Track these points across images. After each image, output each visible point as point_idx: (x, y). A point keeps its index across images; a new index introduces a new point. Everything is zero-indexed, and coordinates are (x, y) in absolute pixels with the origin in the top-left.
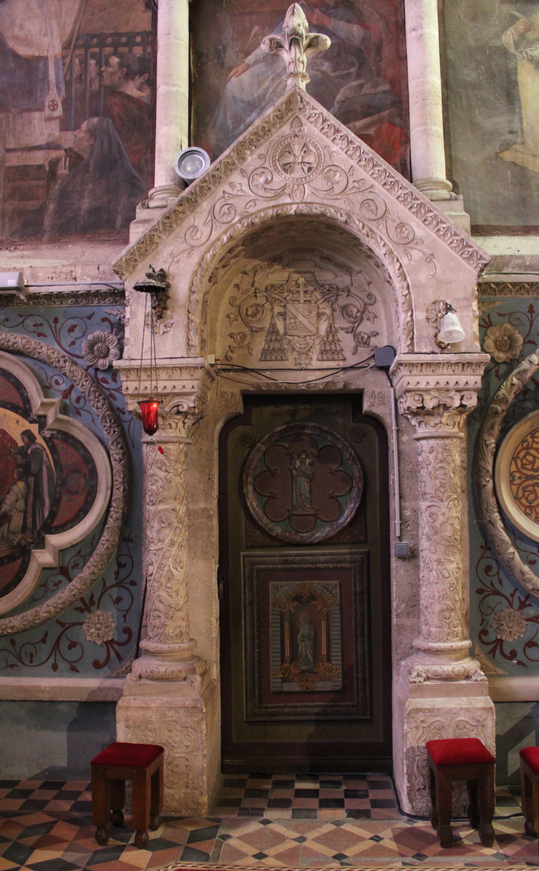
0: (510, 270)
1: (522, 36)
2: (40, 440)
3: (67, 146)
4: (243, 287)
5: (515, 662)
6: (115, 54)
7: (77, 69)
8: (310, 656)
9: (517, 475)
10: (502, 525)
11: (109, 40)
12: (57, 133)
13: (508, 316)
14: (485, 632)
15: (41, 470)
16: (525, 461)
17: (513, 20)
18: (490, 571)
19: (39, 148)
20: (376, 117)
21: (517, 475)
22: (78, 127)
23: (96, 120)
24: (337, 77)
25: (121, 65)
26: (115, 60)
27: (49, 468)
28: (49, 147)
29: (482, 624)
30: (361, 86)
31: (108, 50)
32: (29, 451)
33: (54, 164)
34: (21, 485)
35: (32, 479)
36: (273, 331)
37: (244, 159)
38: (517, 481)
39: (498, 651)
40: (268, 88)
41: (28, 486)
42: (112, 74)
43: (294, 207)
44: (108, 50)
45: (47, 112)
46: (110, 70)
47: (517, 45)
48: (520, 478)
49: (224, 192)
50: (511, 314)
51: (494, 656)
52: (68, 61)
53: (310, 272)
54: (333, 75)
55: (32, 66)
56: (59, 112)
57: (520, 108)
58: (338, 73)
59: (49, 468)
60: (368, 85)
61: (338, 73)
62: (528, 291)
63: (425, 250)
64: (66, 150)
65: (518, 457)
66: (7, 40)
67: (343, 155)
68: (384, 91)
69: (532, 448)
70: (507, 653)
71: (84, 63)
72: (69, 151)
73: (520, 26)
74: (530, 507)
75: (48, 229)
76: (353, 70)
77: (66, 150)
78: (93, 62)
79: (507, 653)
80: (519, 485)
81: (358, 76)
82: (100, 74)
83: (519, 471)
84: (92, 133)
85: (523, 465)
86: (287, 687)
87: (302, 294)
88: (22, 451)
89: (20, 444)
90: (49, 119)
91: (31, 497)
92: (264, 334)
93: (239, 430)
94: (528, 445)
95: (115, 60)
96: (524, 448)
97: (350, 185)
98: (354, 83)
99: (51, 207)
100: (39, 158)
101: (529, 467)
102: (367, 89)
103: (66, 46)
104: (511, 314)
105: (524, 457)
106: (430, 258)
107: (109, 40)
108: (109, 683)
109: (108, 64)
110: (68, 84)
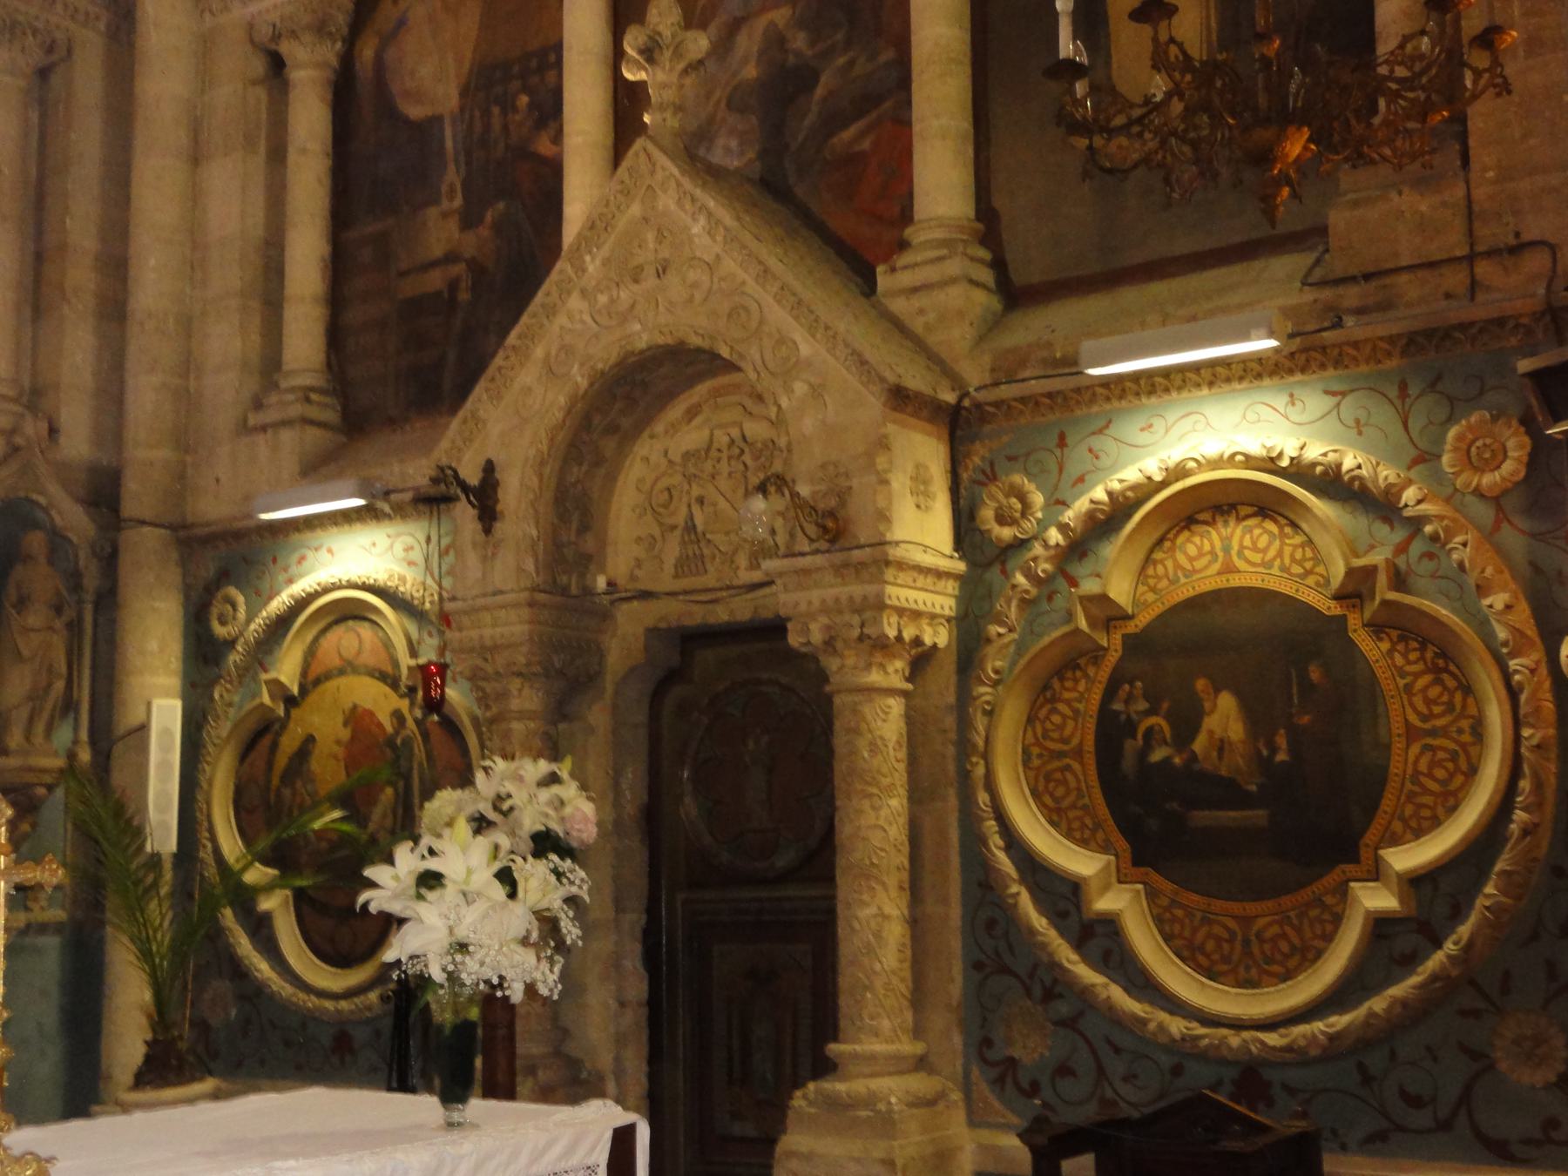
2: (410, 723)
4: (653, 458)
5: (1037, 1102)
7: (478, 126)
8: (769, 1076)
9: (1035, 751)
10: (1001, 843)
11: (516, 69)
14: (987, 1042)
15: (411, 769)
16: (1450, 765)
18: (431, 888)
19: (434, 264)
20: (874, 115)
21: (1035, 751)
22: (481, 221)
23: (501, 205)
27: (421, 764)
28: (450, 258)
29: (982, 1027)
30: (851, 63)
31: (516, 84)
32: (399, 741)
33: (453, 285)
34: (389, 791)
35: (401, 784)
36: (690, 527)
37: (584, 270)
38: (1036, 762)
39: (1009, 1080)
41: (396, 790)
43: (645, 337)
44: (516, 84)
45: (445, 204)
46: (518, 118)
48: (1040, 756)
49: (562, 328)
51: (1002, 1089)
53: (734, 424)
55: (426, 130)
56: (458, 202)
59: (421, 764)
63: (812, 380)
65: (1075, 720)
66: (398, 101)
67: (706, 240)
69: (1060, 700)
70: (1025, 1085)
71: (486, 113)
74: (1059, 811)
78: (496, 110)
79: (1025, 1085)
80: (1038, 769)
82: (505, 128)
83: (1038, 743)
85: (1045, 731)
86: (738, 1129)
87: (724, 462)
88: (390, 742)
89: (389, 729)
90: (445, 215)
91: (400, 811)
92: (678, 533)
93: (677, 692)
94: (1053, 695)
95: (524, 100)
96: (1047, 701)
97: (715, 287)
98: (841, 61)
100: (435, 281)
101: (1441, 755)
103: (464, 92)
105: (1452, 776)
106: (817, 392)
107: (516, 69)
109: (515, 109)
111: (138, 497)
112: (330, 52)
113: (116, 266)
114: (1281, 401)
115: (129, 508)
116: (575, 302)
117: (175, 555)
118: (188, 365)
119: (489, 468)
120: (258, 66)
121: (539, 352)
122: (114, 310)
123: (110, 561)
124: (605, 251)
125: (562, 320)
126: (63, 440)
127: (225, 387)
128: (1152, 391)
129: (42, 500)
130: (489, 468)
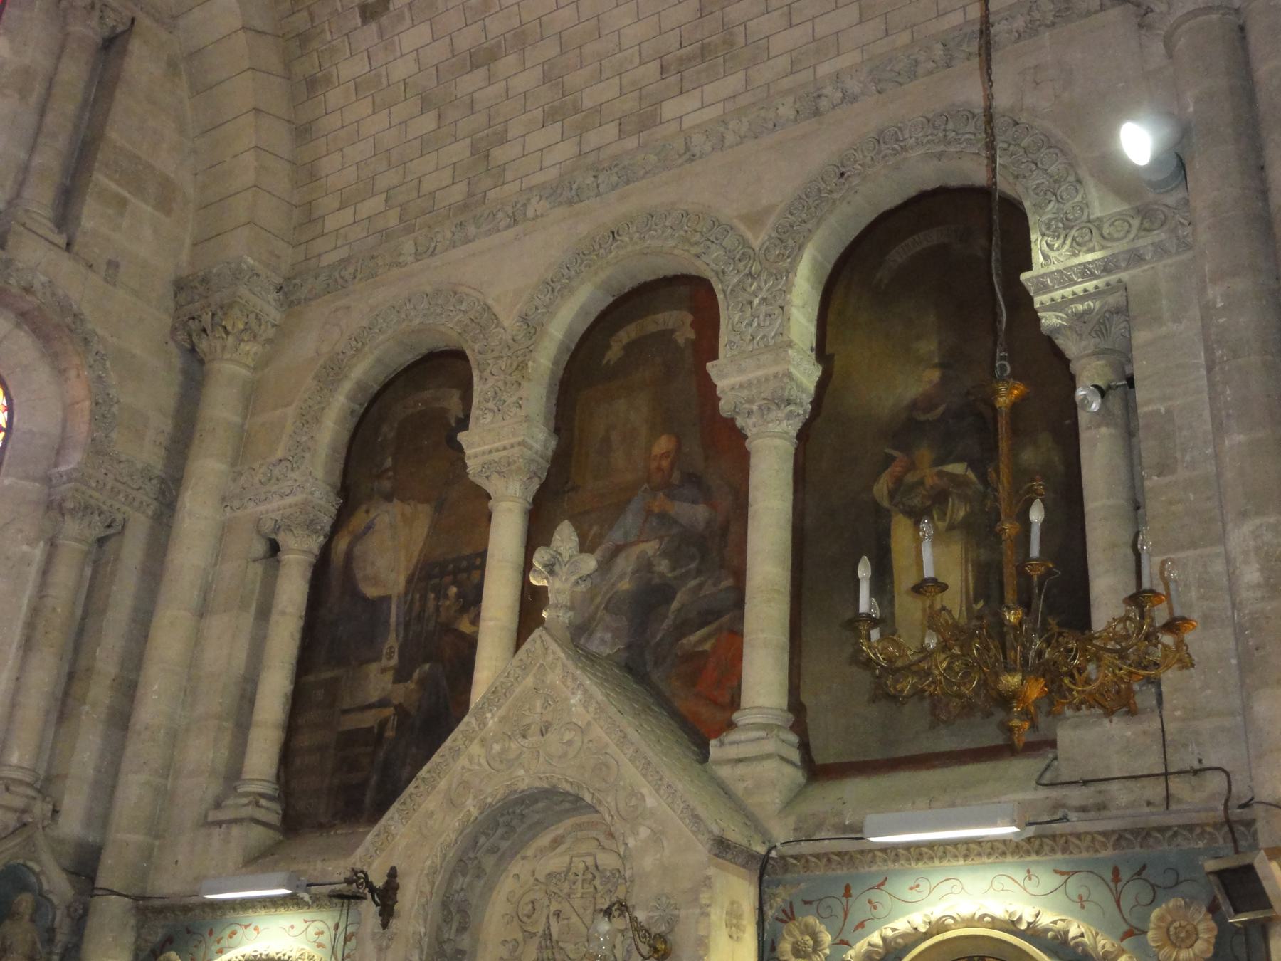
0: (823, 835)
1: (898, 481)
3: (396, 702)
6: (454, 583)
12: (390, 686)
13: (814, 905)
17: (889, 460)
19: (370, 706)
23: (427, 666)
24: (675, 578)
25: (458, 596)
26: (453, 590)
28: (383, 703)
30: (701, 586)
33: (383, 724)
40: (600, 604)
42: (449, 607)
44: (448, 579)
46: (448, 603)
47: (892, 495)
50: (820, 900)
52: (409, 597)
54: (670, 575)
56: (394, 661)
57: (892, 583)
58: (677, 573)
60: (710, 582)
61: (677, 573)
62: (839, 863)
64: (396, 707)
68: (728, 588)
71: (424, 598)
72: (399, 709)
73: (896, 469)
75: (1219, 304)
76: (693, 566)
77: (396, 707)
81: (699, 572)
82: (437, 609)
84: (422, 683)
99: (374, 779)
100: (369, 720)
102: (709, 589)
103: (409, 581)
104: (820, 900)
106: (657, 837)
108: (127, 195)
109: (446, 597)
110: (407, 625)
111: (111, 873)
112: (314, 544)
113: (128, 689)
114: (1020, 875)
115: (103, 880)
116: (475, 749)
117: (132, 922)
118: (169, 769)
119: (393, 874)
120: (260, 548)
121: (443, 784)
122: (121, 720)
123: (80, 921)
124: (502, 712)
125: (463, 761)
126: (61, 820)
127: (197, 789)
128: (919, 858)
129: (37, 868)
130: (393, 874)
